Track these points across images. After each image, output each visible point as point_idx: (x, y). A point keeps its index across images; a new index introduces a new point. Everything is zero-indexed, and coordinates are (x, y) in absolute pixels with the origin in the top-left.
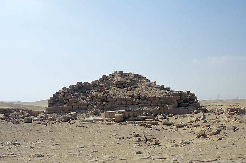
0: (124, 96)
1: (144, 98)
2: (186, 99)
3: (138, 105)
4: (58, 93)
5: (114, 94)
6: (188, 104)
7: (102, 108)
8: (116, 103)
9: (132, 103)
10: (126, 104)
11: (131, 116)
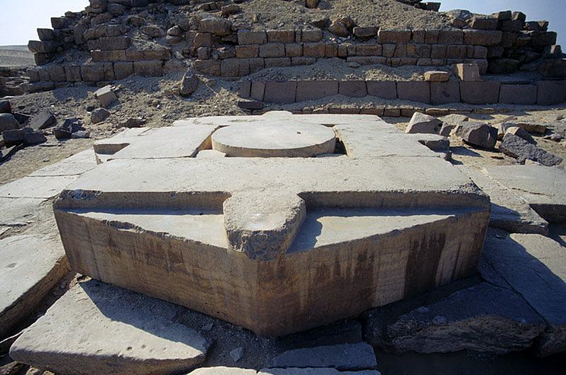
0: (296, 23)
1: (369, 35)
2: (514, 44)
3: (345, 58)
4: (71, 16)
5: (260, 14)
6: (520, 65)
7: (214, 68)
8: (266, 50)
9: (322, 53)
10: (302, 55)
11: (476, 55)
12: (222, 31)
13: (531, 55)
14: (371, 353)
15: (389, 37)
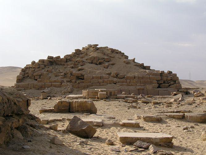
3: (116, 84)
6: (169, 86)
9: (109, 82)
10: (103, 83)
12: (80, 75)
13: (172, 83)
14: (192, 127)
15: (130, 78)
